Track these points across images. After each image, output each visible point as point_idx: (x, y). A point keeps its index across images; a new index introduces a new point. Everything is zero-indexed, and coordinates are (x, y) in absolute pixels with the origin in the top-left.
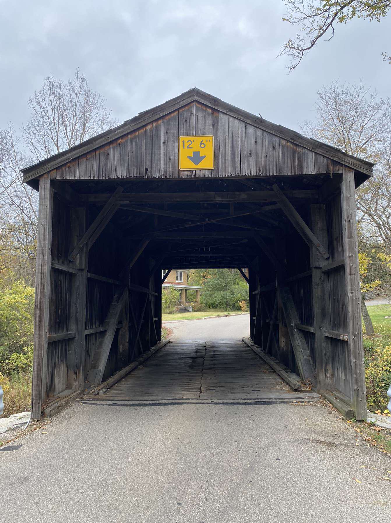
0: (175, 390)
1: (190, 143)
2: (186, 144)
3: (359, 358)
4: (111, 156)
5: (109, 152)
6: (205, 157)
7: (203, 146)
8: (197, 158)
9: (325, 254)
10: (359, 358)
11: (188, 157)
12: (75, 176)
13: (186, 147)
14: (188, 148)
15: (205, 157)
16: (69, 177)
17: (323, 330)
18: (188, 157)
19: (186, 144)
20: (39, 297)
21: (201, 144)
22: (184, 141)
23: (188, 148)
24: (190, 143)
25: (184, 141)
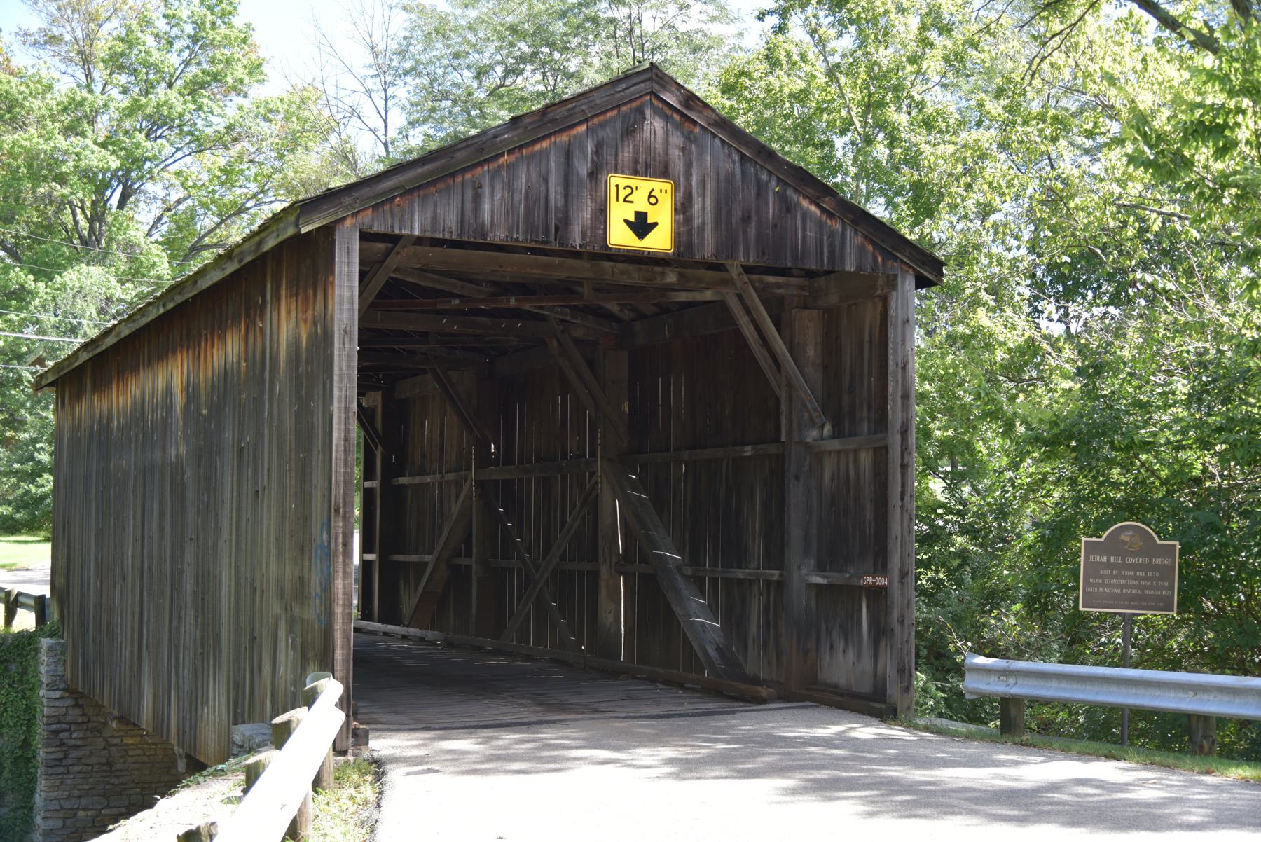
0: (1249, 800)
1: (629, 191)
2: (623, 193)
3: (230, 580)
4: (486, 190)
5: (482, 182)
6: (655, 225)
7: (653, 201)
8: (641, 225)
9: (191, 539)
10: (230, 580)
11: (626, 221)
12: (412, 228)
13: (621, 198)
14: (625, 201)
15: (655, 225)
16: (400, 229)
17: (804, 571)
18: (626, 221)
19: (623, 193)
20: (342, 492)
21: (650, 196)
22: (617, 186)
23: (625, 201)
24: (629, 191)
25: (617, 186)
